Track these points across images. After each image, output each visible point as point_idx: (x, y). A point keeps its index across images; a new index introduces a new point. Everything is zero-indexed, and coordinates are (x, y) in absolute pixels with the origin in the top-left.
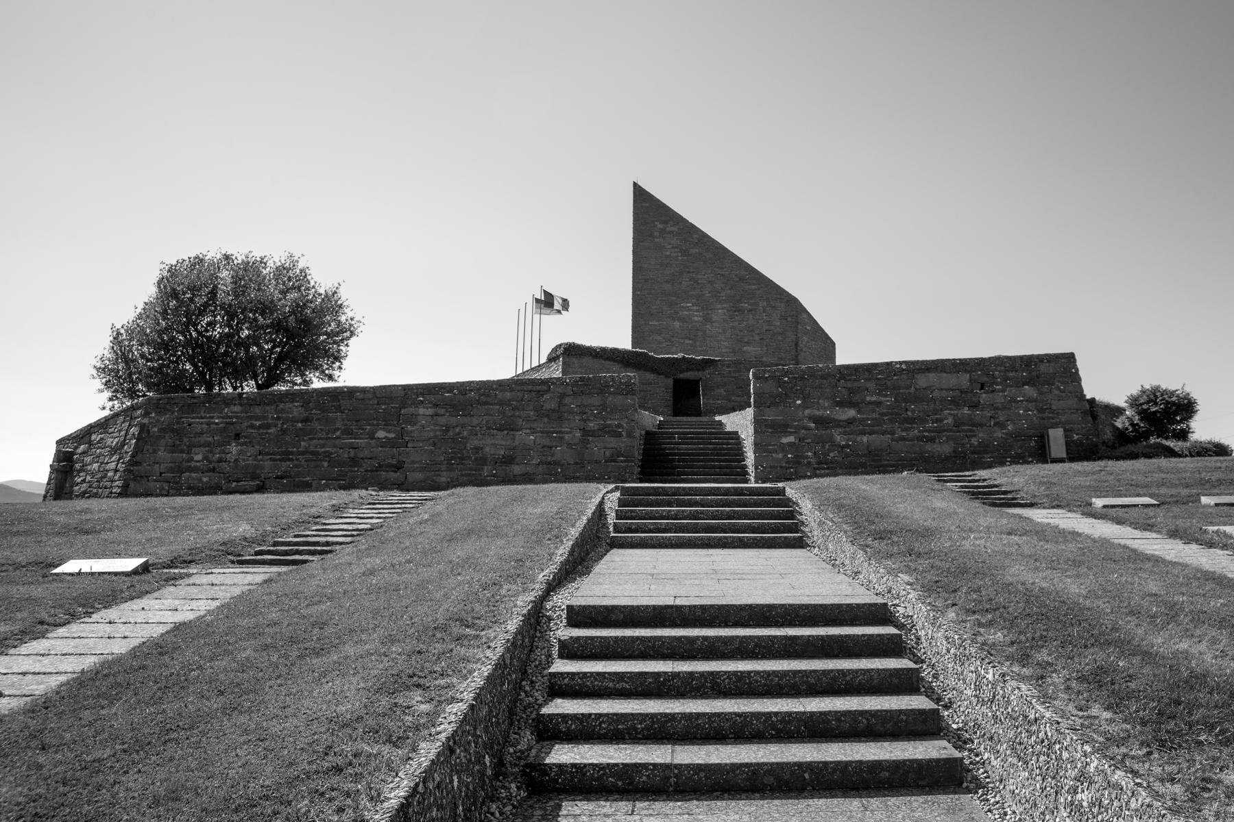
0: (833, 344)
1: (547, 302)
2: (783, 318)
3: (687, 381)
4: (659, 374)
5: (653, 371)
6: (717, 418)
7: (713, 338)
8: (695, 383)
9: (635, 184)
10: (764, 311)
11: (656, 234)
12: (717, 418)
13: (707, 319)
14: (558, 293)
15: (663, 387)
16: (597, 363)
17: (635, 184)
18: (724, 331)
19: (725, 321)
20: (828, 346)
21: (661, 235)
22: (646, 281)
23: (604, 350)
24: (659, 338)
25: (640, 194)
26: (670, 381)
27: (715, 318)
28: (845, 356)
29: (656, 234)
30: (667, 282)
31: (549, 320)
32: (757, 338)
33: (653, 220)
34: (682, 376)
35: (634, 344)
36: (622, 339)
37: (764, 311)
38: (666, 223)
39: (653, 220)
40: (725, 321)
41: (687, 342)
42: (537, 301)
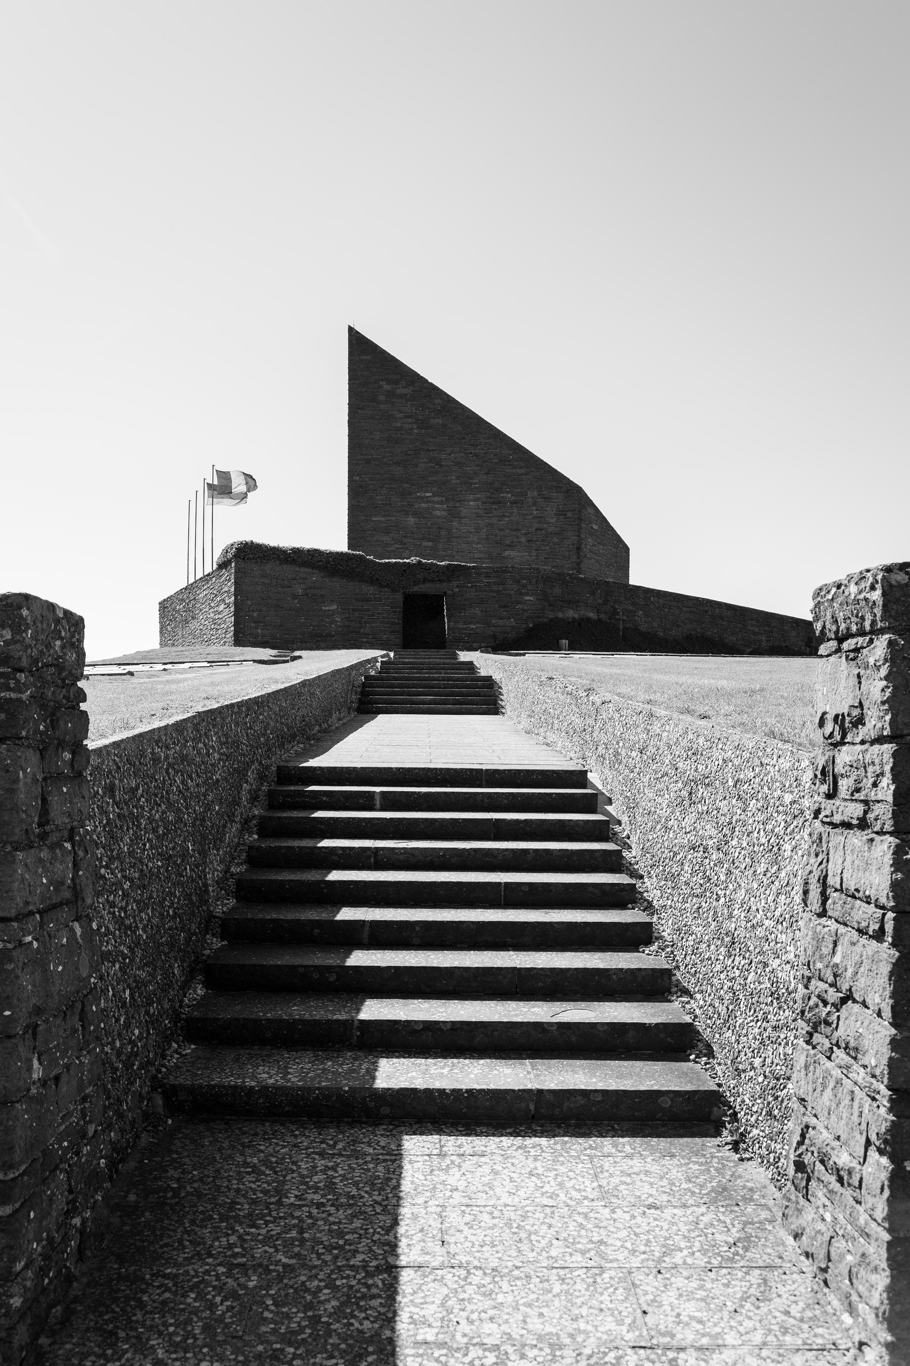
0: (627, 550)
1: (221, 488)
2: (561, 513)
3: (425, 596)
4: (382, 586)
5: (373, 581)
6: (464, 656)
7: (464, 540)
8: (438, 599)
9: (351, 329)
10: (535, 504)
11: (382, 398)
12: (464, 656)
13: (454, 514)
14: (234, 467)
15: (387, 607)
16: (289, 570)
17: (351, 329)
18: (478, 530)
19: (479, 516)
20: (619, 552)
21: (394, 412)
22: (368, 462)
23: (297, 552)
24: (386, 539)
25: (362, 350)
26: (399, 597)
27: (464, 512)
28: (638, 576)
29: (382, 398)
30: (397, 463)
31: (224, 508)
32: (523, 539)
33: (375, 375)
34: (416, 589)
35: (350, 546)
36: (330, 533)
37: (535, 504)
38: (396, 382)
39: (375, 375)
40: (479, 516)
41: (425, 543)
42: (211, 487)
